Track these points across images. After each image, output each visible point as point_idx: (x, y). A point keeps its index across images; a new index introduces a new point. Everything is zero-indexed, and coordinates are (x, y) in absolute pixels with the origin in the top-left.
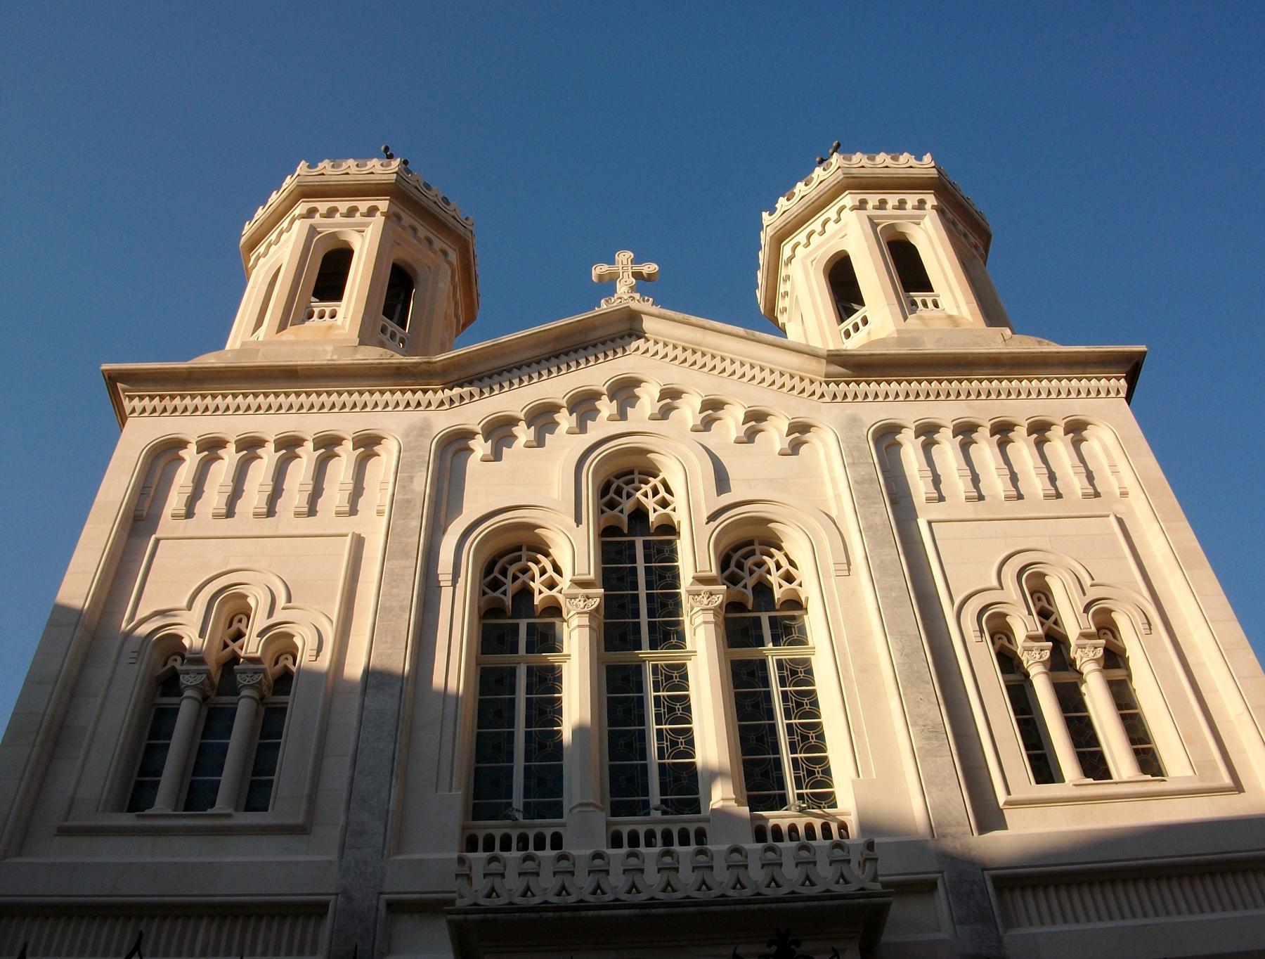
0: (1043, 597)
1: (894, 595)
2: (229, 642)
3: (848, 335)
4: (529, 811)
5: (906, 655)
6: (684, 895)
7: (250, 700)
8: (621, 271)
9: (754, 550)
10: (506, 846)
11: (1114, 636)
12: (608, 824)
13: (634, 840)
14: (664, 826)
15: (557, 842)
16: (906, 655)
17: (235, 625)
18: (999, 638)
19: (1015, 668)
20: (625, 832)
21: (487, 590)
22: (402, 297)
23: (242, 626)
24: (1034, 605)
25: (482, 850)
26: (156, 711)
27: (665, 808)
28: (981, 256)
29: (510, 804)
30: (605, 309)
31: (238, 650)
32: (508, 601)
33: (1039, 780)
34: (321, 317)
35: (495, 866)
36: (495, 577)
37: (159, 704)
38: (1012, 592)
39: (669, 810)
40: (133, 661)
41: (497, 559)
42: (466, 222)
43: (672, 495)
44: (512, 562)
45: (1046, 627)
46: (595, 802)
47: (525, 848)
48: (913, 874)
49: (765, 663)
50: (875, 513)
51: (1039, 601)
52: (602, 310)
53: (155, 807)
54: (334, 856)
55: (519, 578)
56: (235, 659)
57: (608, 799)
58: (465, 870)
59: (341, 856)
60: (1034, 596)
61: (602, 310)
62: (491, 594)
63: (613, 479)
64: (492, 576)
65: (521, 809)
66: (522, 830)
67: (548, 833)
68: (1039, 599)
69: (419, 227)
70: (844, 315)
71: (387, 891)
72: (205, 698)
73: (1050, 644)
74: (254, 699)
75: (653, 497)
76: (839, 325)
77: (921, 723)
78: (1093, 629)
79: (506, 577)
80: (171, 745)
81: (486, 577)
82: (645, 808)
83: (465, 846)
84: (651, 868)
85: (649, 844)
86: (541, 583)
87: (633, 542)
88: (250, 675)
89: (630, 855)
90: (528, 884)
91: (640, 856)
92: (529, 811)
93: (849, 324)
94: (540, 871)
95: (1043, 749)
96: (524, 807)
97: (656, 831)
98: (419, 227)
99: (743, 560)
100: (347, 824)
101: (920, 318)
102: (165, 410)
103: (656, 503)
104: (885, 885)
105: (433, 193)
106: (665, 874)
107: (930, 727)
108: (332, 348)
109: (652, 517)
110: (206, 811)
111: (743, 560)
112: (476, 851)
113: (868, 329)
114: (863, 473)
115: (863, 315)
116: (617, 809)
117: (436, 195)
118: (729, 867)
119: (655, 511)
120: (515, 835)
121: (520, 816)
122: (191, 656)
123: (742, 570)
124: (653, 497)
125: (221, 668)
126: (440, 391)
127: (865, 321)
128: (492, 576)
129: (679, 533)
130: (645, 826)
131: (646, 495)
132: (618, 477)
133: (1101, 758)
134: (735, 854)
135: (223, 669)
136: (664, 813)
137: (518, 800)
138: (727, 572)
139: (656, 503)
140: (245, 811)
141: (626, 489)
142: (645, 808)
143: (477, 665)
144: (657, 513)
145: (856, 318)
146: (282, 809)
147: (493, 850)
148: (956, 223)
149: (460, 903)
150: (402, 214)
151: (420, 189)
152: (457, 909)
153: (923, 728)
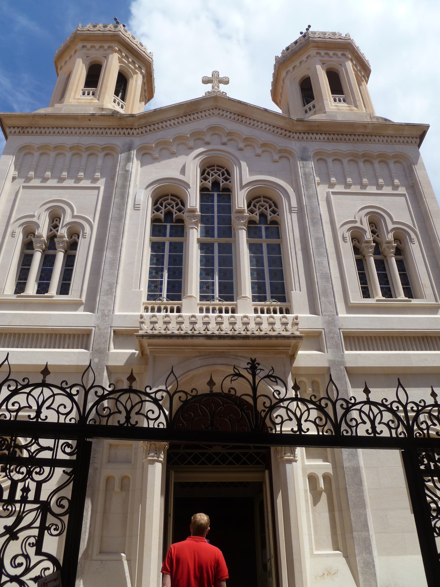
0: (374, 226)
3: (306, 112)
5: (317, 245)
6: (225, 333)
8: (214, 79)
11: (400, 243)
16: (317, 245)
17: (55, 222)
18: (355, 241)
19: (360, 253)
22: (122, 87)
23: (57, 223)
24: (370, 229)
27: (220, 299)
31: (56, 232)
32: (162, 216)
34: (88, 94)
36: (158, 206)
38: (366, 226)
39: (222, 300)
41: (159, 199)
42: (149, 54)
43: (230, 176)
47: (167, 312)
49: (263, 214)
55: (167, 207)
60: (370, 225)
63: (206, 168)
68: (372, 226)
70: (306, 103)
71: (114, 326)
75: (222, 177)
76: (303, 108)
79: (256, 207)
82: (213, 298)
85: (213, 312)
86: (176, 209)
87: (166, 225)
93: (307, 106)
95: (409, 285)
99: (256, 204)
103: (223, 179)
104: (301, 332)
105: (127, 34)
108: (93, 108)
109: (221, 185)
111: (256, 204)
113: (315, 110)
115: (309, 106)
117: (129, 35)
120: (162, 307)
121: (165, 300)
123: (256, 207)
124: (222, 177)
125: (26, 245)
126: (137, 129)
127: (314, 107)
128: (157, 206)
129: (232, 191)
131: (219, 175)
132: (208, 168)
133: (390, 290)
135: (50, 240)
136: (220, 301)
138: (250, 208)
139: (223, 179)
140: (60, 294)
141: (212, 172)
142: (213, 298)
143: (150, 241)
145: (310, 105)
146: (73, 296)
149: (141, 332)
151: (130, 38)
152: (140, 334)
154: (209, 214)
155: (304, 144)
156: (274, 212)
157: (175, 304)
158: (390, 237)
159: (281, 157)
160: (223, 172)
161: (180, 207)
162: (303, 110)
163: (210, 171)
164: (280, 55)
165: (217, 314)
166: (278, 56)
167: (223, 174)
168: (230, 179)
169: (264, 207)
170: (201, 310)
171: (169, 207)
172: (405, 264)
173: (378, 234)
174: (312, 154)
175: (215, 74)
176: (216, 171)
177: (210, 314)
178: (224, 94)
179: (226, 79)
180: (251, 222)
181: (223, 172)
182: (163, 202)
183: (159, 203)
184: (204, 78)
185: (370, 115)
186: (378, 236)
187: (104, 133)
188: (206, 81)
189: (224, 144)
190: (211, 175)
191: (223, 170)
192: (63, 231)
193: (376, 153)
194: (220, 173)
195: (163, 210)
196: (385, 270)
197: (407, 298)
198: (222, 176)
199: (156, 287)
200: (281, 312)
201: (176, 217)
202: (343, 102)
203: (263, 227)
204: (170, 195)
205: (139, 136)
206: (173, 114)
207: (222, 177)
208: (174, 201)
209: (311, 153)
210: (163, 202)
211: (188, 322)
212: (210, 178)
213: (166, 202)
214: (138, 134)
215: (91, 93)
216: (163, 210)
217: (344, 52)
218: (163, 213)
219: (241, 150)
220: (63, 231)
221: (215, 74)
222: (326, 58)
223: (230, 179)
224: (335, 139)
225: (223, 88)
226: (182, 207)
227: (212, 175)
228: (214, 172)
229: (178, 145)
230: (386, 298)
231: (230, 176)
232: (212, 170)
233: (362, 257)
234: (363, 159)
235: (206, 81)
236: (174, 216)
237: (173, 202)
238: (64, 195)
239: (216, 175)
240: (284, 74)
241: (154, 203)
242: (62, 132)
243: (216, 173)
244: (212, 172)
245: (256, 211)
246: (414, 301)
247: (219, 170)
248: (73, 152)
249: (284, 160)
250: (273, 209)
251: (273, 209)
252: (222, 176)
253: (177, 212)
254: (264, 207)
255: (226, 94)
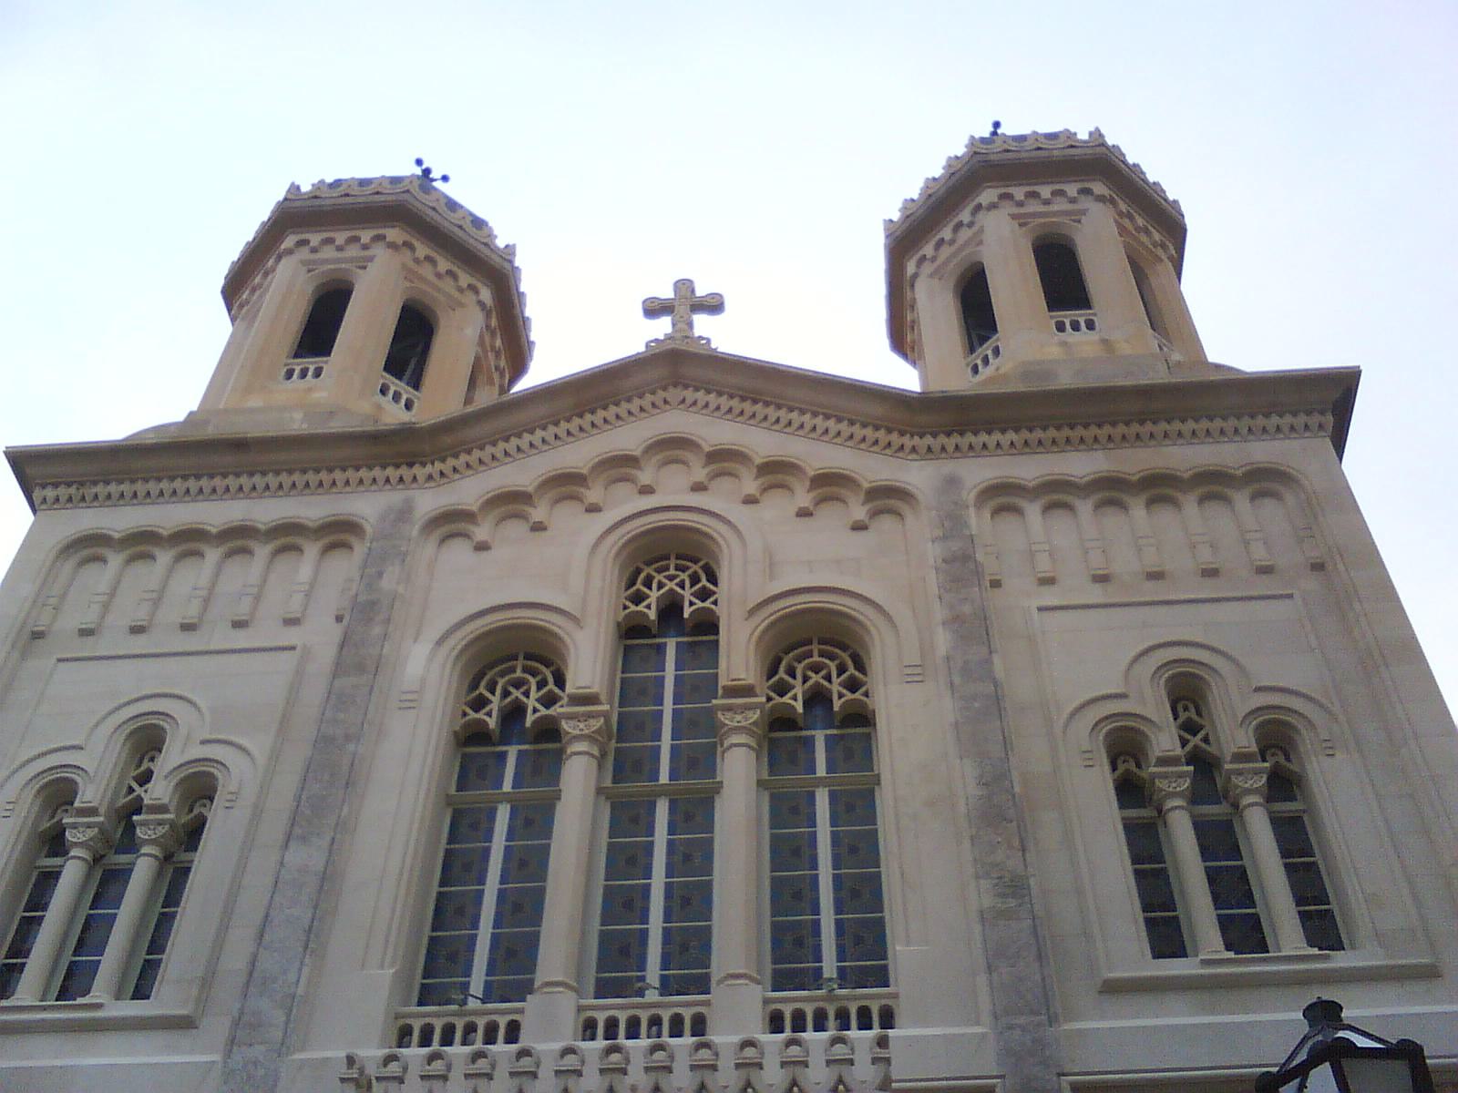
1: (976, 705)
2: (135, 785)
4: (666, 987)
7: (153, 859)
9: (811, 651)
10: (676, 1031)
12: (766, 1001)
13: (611, 1029)
14: (816, 1005)
15: (699, 1026)
17: (145, 765)
20: (788, 1011)
21: (468, 710)
25: (812, 1029)
26: (39, 875)
28: (1171, 258)
29: (642, 979)
30: (312, 363)
31: (143, 795)
32: (492, 723)
33: (1158, 954)
34: (304, 374)
35: (840, 1051)
36: (481, 694)
37: (42, 867)
40: (8, 814)
44: (502, 674)
45: (1189, 747)
46: (568, 981)
48: (927, 1080)
50: (966, 599)
51: (1185, 711)
52: (316, 363)
53: (91, 994)
54: (216, 1057)
55: (810, 678)
56: (137, 807)
57: (768, 967)
58: (883, 1053)
59: (228, 1053)
61: (316, 363)
62: (473, 715)
63: (642, 566)
64: (477, 692)
65: (657, 986)
66: (468, 1019)
67: (687, 1014)
69: (417, 244)
72: (97, 859)
73: (1191, 768)
74: (156, 857)
77: (995, 876)
78: (1254, 748)
79: (794, 677)
80: (486, 891)
81: (769, 678)
83: (767, 1026)
84: (817, 1060)
85: (819, 1027)
88: (152, 827)
89: (836, 1041)
90: (657, 1083)
91: (579, 1052)
92: (666, 987)
94: (406, 1077)
95: (1175, 910)
96: (838, 973)
97: (806, 1010)
98: (417, 244)
100: (242, 1013)
101: (1064, 344)
102: (876, 442)
106: (836, 1069)
107: (1006, 880)
110: (75, 1000)
112: (680, 1036)
114: (954, 549)
116: (782, 981)
118: (738, 1066)
119: (691, 604)
120: (644, 1017)
122: (82, 805)
123: (794, 677)
130: (486, 1016)
131: (682, 585)
132: (649, 564)
133: (1255, 923)
134: (837, 1045)
137: (653, 972)
140: (132, 999)
141: (658, 577)
144: (694, 607)
146: (166, 999)
147: (615, 1038)
148: (1132, 215)
150: (1087, 185)
153: (996, 881)
154: (648, 708)
155: (949, 467)
156: (853, 685)
157: (685, 1005)
158: (1245, 740)
159: (875, 513)
160: (696, 572)
161: (551, 691)
162: (968, 365)
163: (654, 574)
164: (896, 216)
165: (600, 1044)
166: (891, 221)
167: (695, 579)
168: (714, 593)
169: (823, 673)
170: (776, 1023)
171: (516, 693)
172: (1310, 830)
173: (1207, 734)
174: (973, 495)
175: (684, 286)
176: (672, 572)
177: (809, 1035)
178: (704, 342)
179: (713, 298)
180: (780, 722)
181: (696, 572)
182: (796, 664)
183: (483, 683)
184: (648, 303)
185: (1166, 360)
186: (1206, 740)
187: (381, 481)
188: (654, 309)
189: (698, 488)
190: (654, 586)
191: (695, 568)
192: (160, 790)
193: (1238, 469)
194: (684, 576)
195: (496, 702)
196: (1236, 852)
197: (1316, 951)
198: (692, 585)
199: (684, 948)
200: (425, 1041)
201: (535, 723)
202: (1088, 331)
203: (820, 737)
204: (521, 657)
205: (432, 484)
206: (542, 410)
207: (691, 587)
208: (832, 657)
209: (968, 494)
210: (796, 664)
211: (778, 1060)
212: (654, 595)
213: (509, 680)
214: (430, 477)
215: (1083, 325)
216: (496, 702)
217: (1087, 185)
218: (800, 697)
219: (750, 501)
220: (160, 790)
221: (684, 286)
222: (1034, 207)
223: (714, 593)
224: (1286, 429)
225: (703, 325)
226: (557, 690)
227: (661, 586)
228: (667, 577)
229: (557, 501)
230: (1320, 949)
231: (715, 584)
232: (659, 571)
233: (1230, 810)
234: (1247, 492)
235: (654, 309)
236: (837, 705)
237: (530, 678)
238: (149, 676)
239: (670, 585)
240: (911, 268)
241: (766, 669)
242: (251, 486)
243: (671, 578)
244: (658, 577)
245: (793, 687)
246: (1340, 960)
247: (683, 569)
248: (326, 541)
249: (887, 522)
250: (852, 677)
251: (852, 677)
252: (692, 585)
253: (538, 706)
254: (823, 673)
255: (708, 340)
